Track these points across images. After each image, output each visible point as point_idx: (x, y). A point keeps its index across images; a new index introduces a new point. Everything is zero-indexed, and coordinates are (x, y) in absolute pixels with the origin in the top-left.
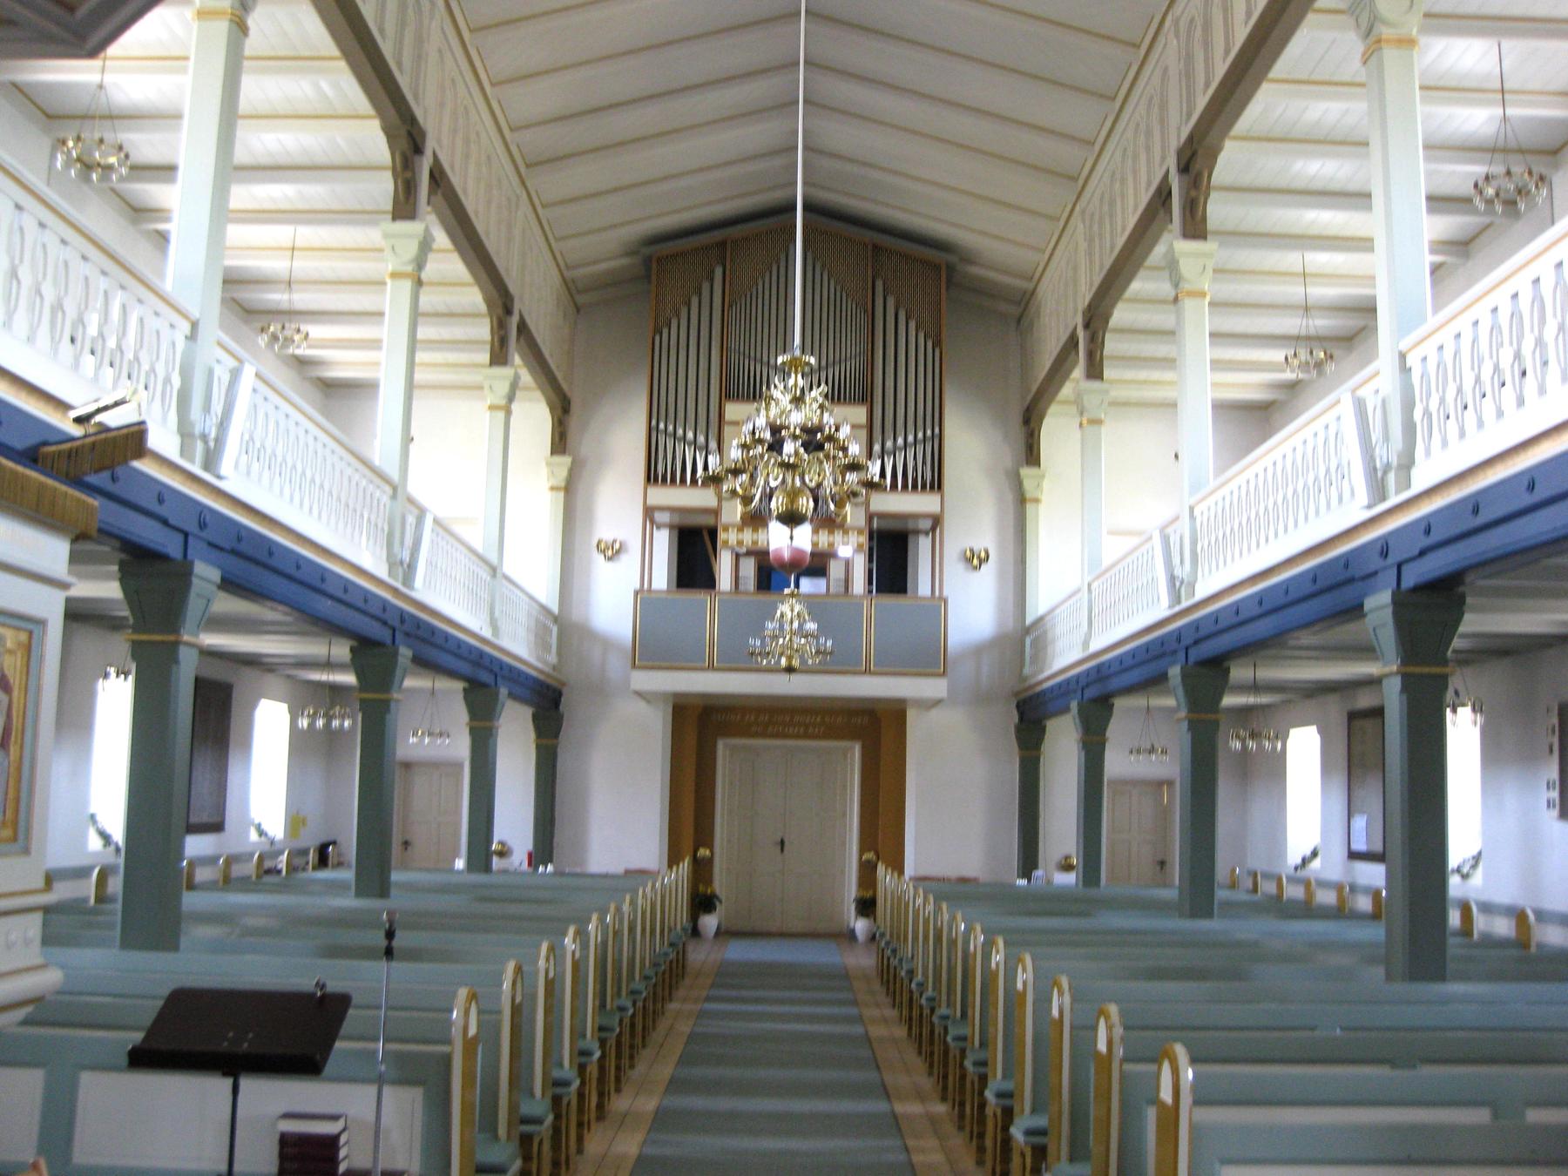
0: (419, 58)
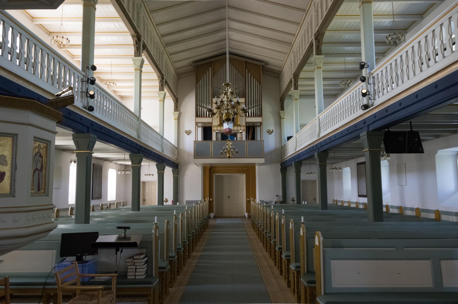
0: (138, 17)
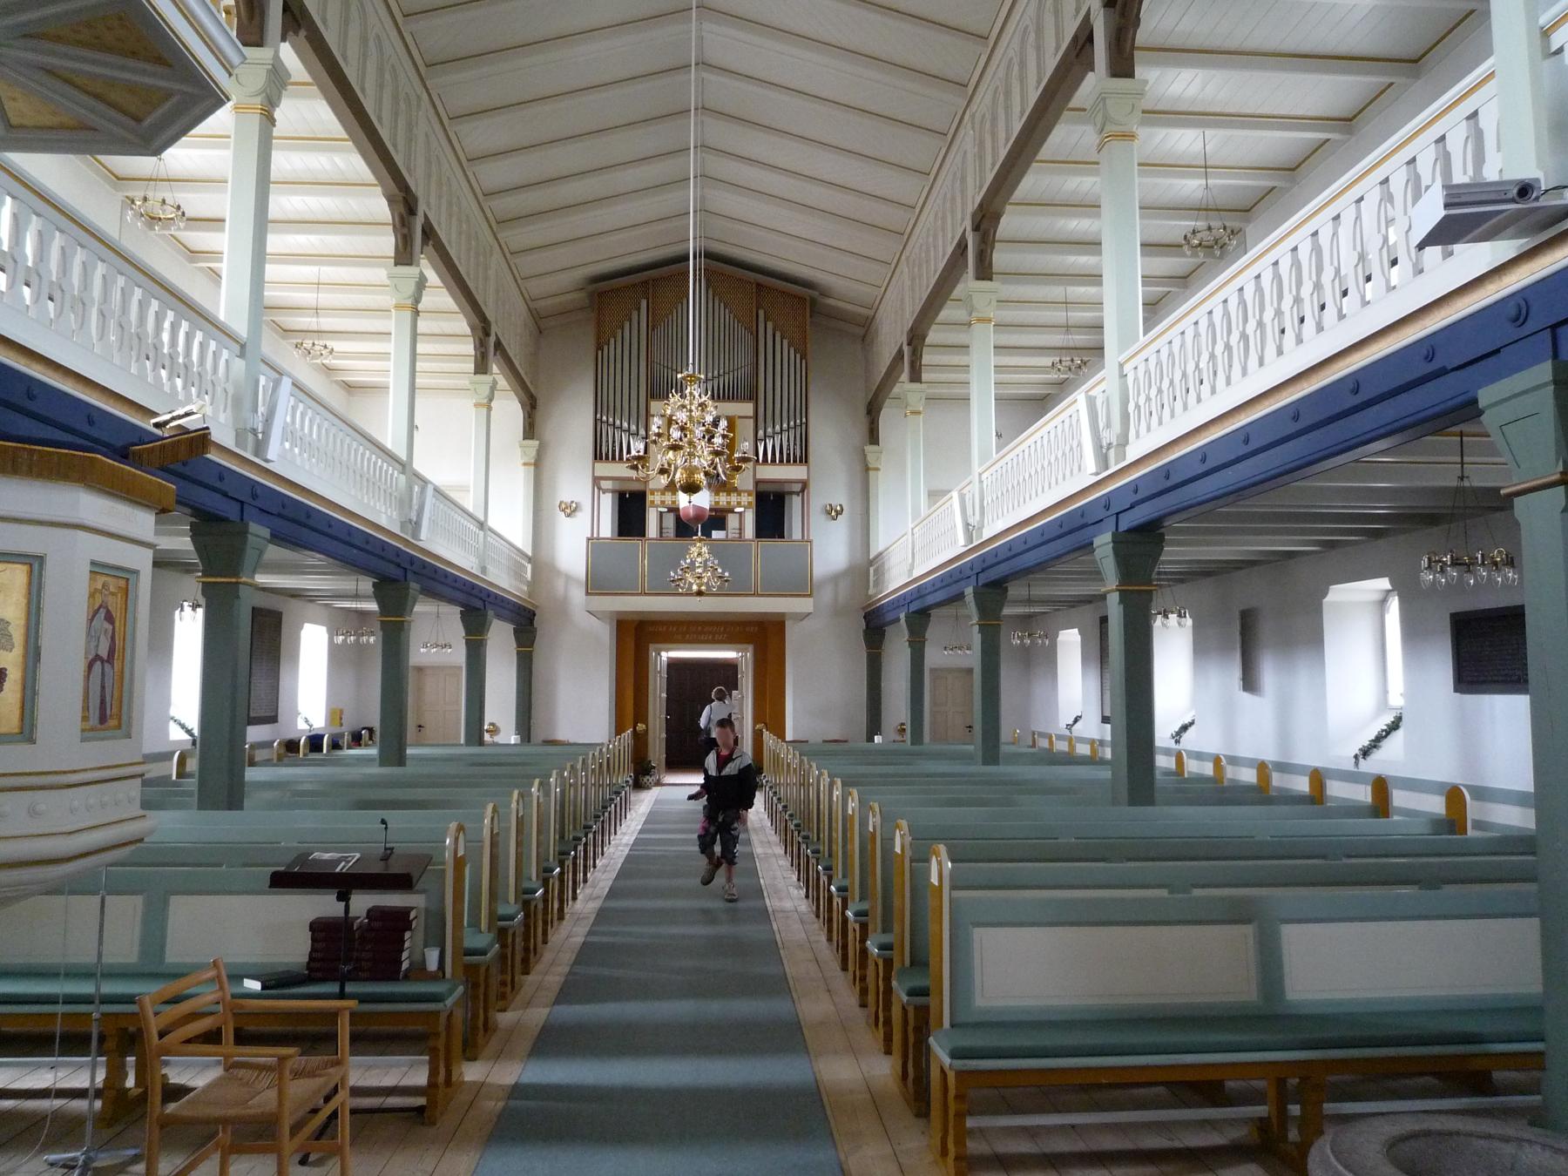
0: (410, 139)
